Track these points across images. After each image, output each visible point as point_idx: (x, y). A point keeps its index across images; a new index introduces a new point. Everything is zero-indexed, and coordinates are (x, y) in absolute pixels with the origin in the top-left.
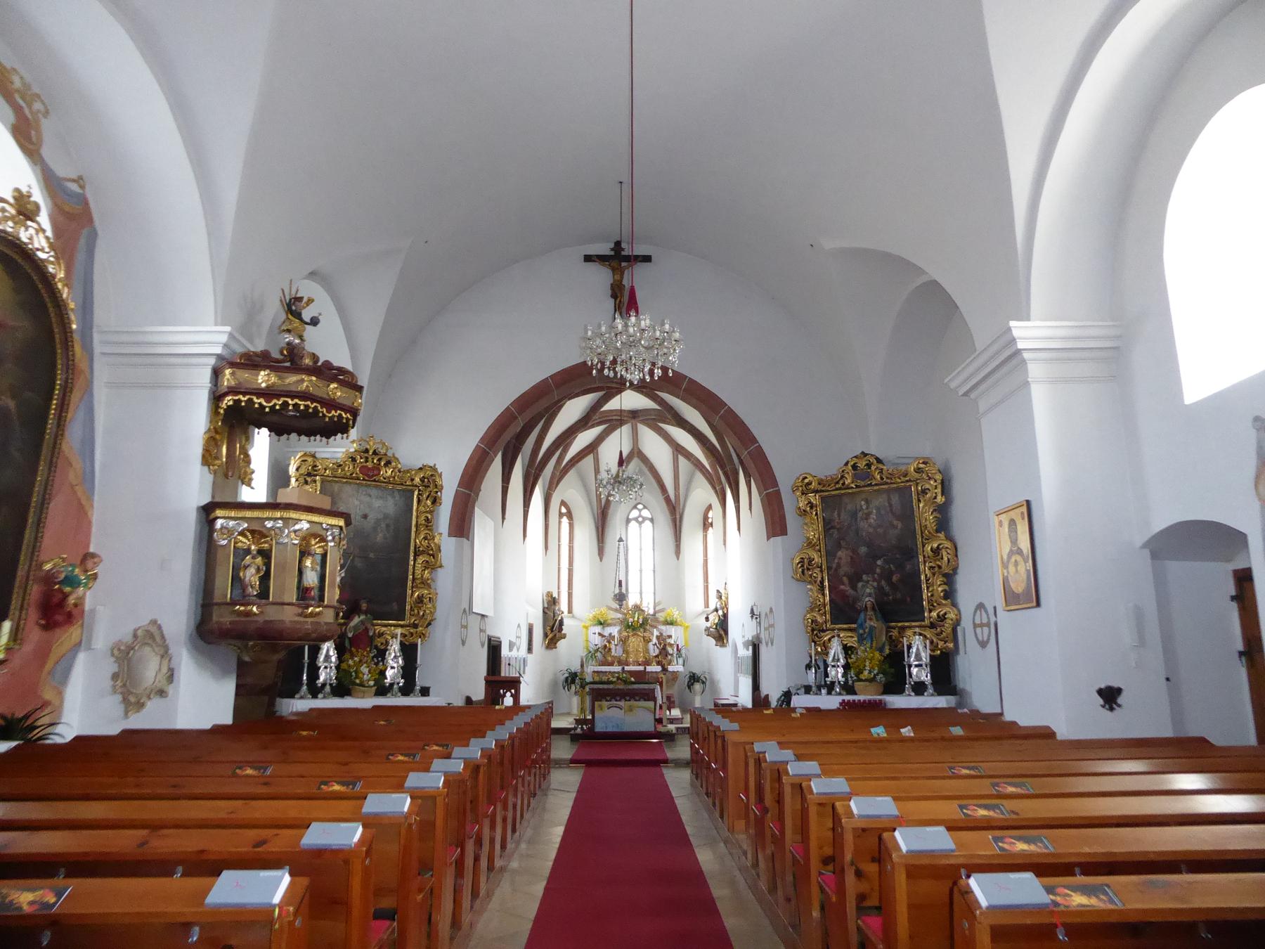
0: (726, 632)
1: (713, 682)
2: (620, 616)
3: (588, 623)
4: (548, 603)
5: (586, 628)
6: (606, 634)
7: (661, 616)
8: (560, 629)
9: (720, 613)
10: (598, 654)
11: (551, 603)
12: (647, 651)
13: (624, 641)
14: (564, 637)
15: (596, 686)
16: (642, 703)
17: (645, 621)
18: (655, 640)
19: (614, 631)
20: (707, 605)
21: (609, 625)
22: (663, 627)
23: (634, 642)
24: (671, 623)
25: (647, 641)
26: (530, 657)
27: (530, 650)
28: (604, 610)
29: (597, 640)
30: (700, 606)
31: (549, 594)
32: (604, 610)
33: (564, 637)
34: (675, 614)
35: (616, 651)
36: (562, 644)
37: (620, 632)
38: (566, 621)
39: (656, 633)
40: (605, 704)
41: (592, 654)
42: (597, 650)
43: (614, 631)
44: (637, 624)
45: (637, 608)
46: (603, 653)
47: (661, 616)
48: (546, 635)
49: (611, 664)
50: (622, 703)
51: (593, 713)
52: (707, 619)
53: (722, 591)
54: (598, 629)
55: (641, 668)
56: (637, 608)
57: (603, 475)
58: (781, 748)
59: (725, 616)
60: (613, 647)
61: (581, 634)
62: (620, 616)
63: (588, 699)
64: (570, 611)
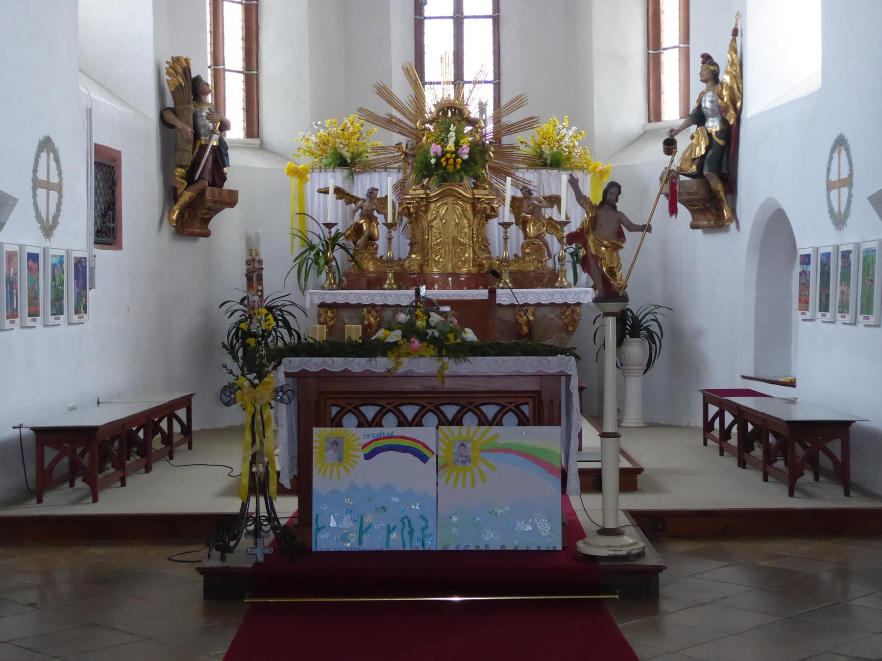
0: (731, 186)
1: (679, 335)
2: (397, 138)
3: (305, 161)
4: (177, 92)
5: (299, 174)
6: (360, 190)
7: (523, 142)
8: (218, 177)
9: (713, 125)
10: (338, 253)
11: (185, 97)
12: (484, 245)
13: (413, 214)
14: (231, 200)
15: (315, 364)
16: (510, 433)
17: (479, 150)
18: (506, 214)
19: (386, 183)
20: (654, 111)
21: (369, 167)
22: (530, 176)
23: (447, 217)
24: (556, 163)
25: (484, 213)
26: (104, 259)
27: (107, 231)
28: (352, 121)
29: (332, 210)
30: (630, 114)
31: (180, 68)
32: (352, 121)
33: (231, 200)
34: (569, 135)
35: (391, 243)
36: (227, 224)
37: (400, 188)
38: (234, 157)
39: (510, 190)
40: (354, 435)
41: (315, 255)
42: (332, 243)
43: (386, 183)
44: (452, 161)
45: (453, 113)
46: (344, 253)
47: (523, 142)
48: (171, 195)
49: (376, 283)
50: (426, 433)
51: (302, 486)
52: (670, 146)
53: (722, 59)
54: (334, 179)
55: (482, 294)
56: (453, 113)
57: (351, 252)
58: (119, 153)
59: (730, 134)
60: (381, 231)
61: (280, 187)
62: (397, 138)
63: (281, 421)
64: (253, 127)
